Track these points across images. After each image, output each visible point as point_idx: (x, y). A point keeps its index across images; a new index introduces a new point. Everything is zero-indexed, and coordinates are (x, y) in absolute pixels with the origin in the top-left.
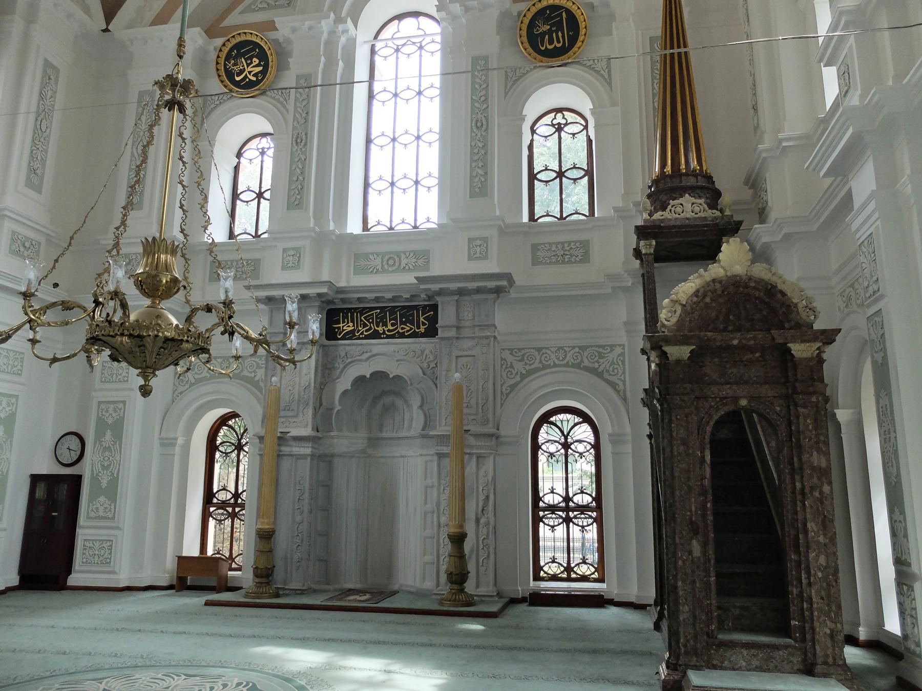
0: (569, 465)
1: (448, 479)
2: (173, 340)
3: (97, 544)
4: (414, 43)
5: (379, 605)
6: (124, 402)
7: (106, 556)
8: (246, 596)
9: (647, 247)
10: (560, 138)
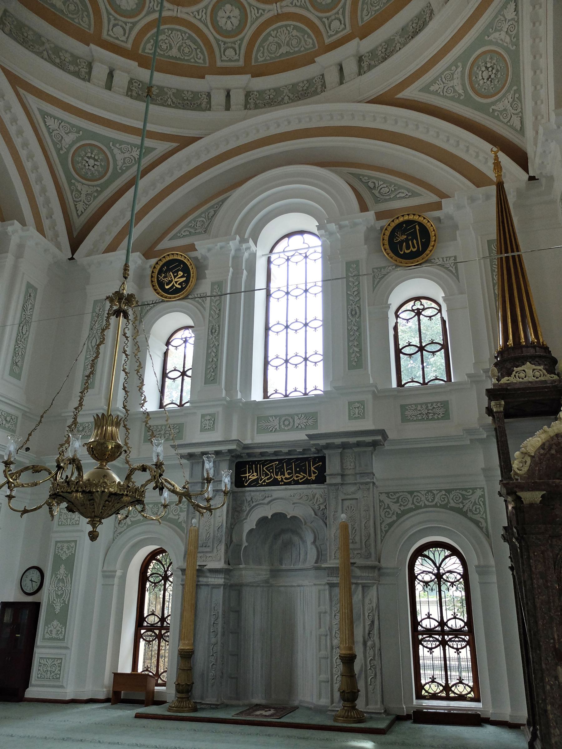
0: (443, 593)
1: (338, 605)
2: (116, 494)
3: (50, 662)
4: (300, 254)
5: (283, 720)
6: (75, 542)
7: (56, 672)
8: (169, 710)
9: (498, 406)
10: (419, 320)
